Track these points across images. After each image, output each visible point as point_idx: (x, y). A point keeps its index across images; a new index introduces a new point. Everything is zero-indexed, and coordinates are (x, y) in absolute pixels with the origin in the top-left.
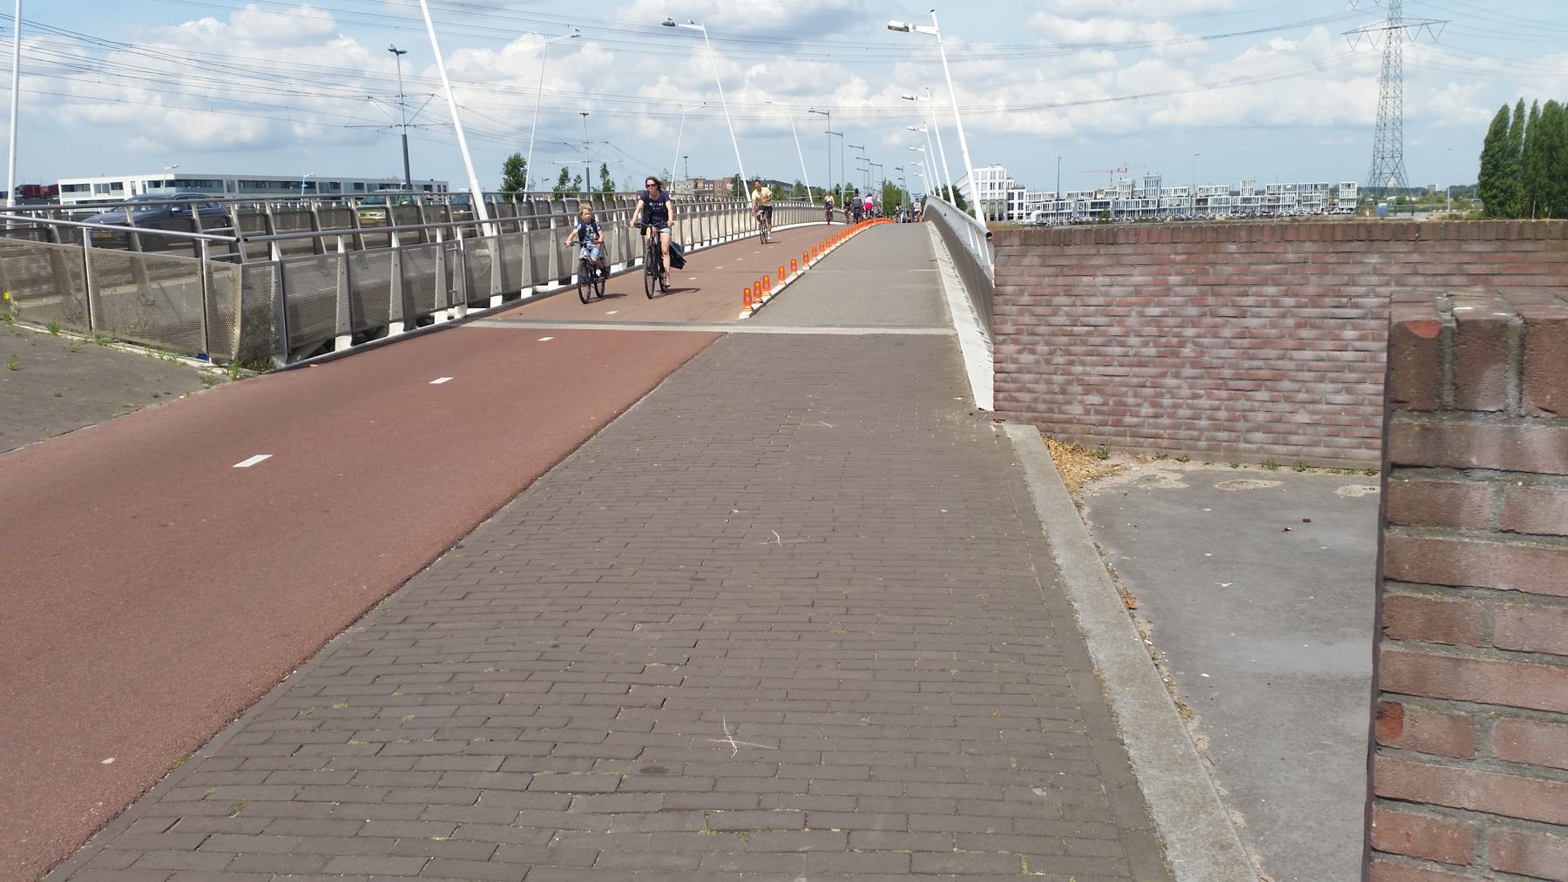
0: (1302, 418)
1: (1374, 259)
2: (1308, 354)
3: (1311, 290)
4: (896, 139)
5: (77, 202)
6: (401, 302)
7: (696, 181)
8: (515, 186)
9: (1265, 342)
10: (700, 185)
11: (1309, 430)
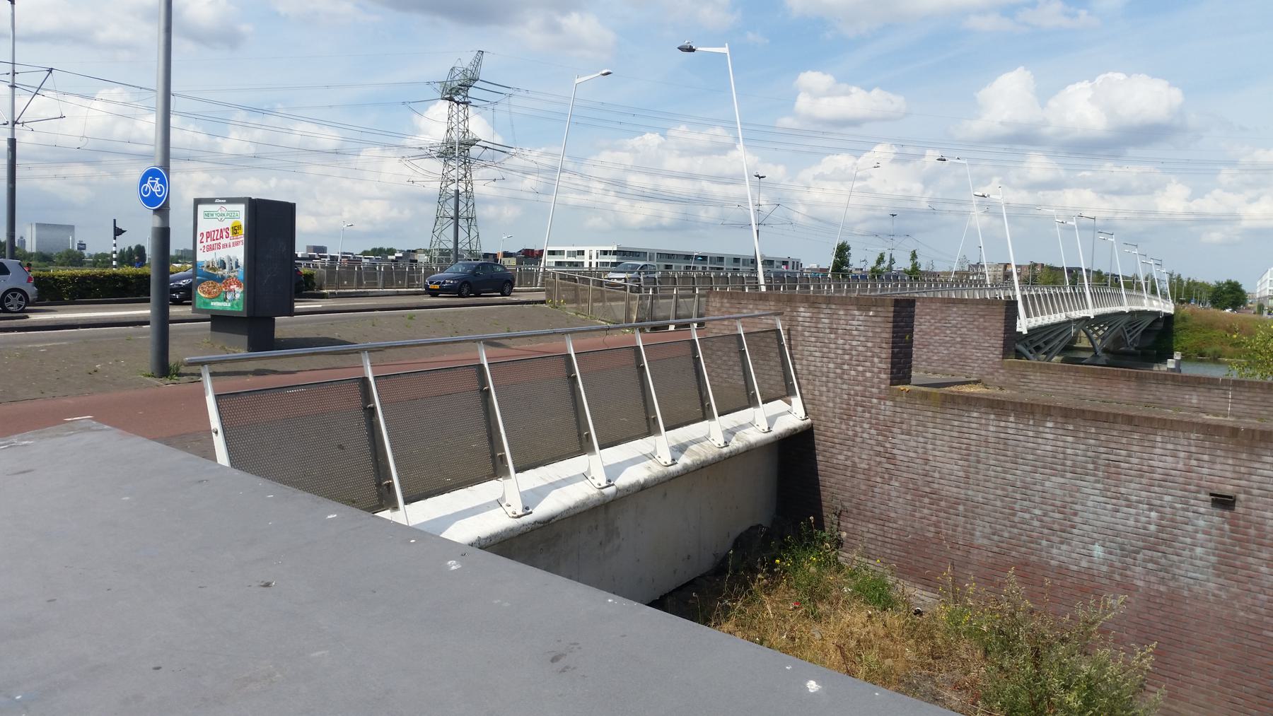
0: (935, 358)
1: (955, 309)
2: (937, 338)
3: (939, 318)
4: (1216, 236)
8: (840, 265)
9: (926, 334)
11: (937, 362)
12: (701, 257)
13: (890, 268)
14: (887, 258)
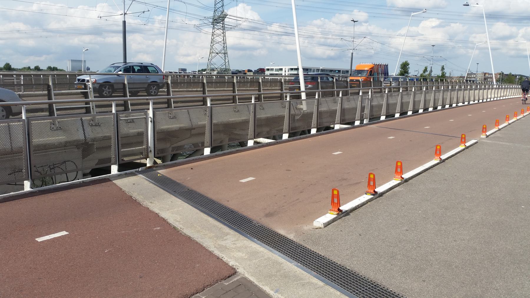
5: (270, 74)
6: (386, 109)
7: (485, 74)
8: (404, 73)
10: (487, 75)
12: (338, 70)
13: (430, 74)
14: (429, 69)
